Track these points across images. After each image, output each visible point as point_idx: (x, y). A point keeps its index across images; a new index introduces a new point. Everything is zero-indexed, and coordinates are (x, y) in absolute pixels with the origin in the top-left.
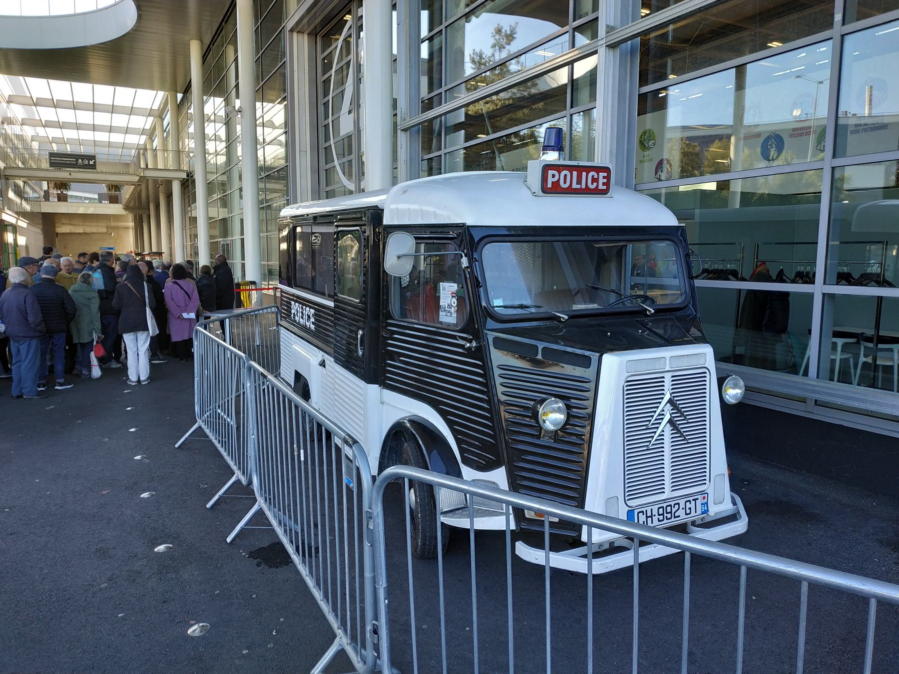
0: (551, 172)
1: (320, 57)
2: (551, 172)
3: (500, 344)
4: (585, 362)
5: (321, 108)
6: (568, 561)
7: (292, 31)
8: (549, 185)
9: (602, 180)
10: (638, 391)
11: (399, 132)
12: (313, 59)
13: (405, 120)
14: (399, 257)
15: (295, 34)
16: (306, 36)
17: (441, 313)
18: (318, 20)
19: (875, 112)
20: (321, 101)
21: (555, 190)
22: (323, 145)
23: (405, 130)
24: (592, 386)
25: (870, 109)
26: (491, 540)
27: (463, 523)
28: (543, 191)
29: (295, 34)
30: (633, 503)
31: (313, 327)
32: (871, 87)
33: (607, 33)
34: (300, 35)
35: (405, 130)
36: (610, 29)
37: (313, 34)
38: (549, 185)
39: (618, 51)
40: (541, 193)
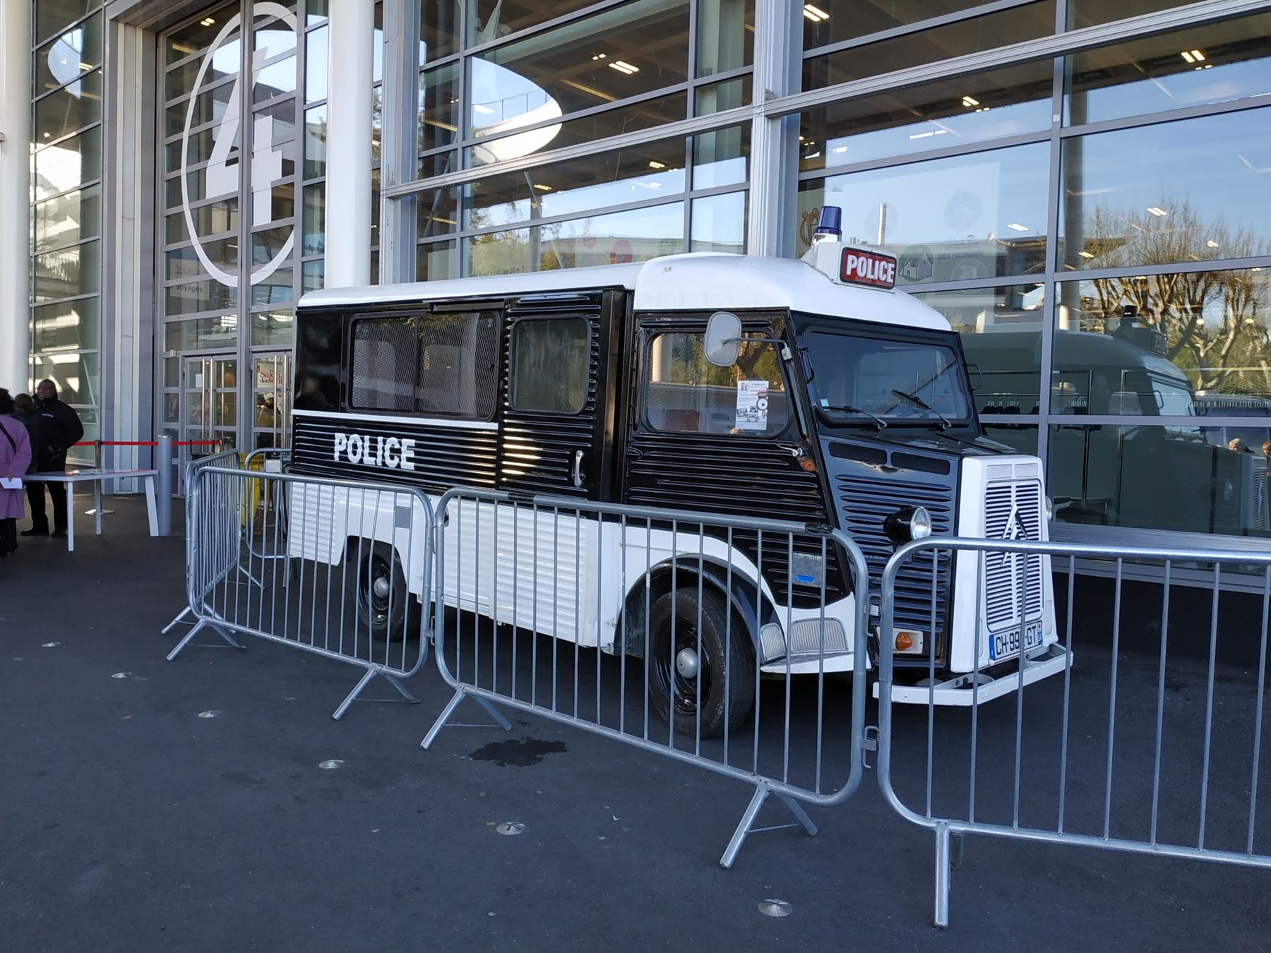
0: (851, 257)
1: (164, 69)
2: (851, 257)
3: (837, 450)
4: (943, 468)
5: (163, 153)
6: (947, 696)
7: (115, 20)
8: (849, 273)
9: (890, 273)
10: (996, 497)
11: (383, 201)
12: (151, 72)
13: (393, 183)
14: (725, 343)
15: (121, 27)
16: (140, 34)
17: (737, 419)
18: (162, 16)
19: (888, 241)
20: (163, 140)
21: (849, 278)
22: (164, 211)
23: (393, 198)
24: (952, 494)
25: (883, 237)
26: (839, 683)
27: (811, 668)
28: (842, 279)
29: (121, 27)
30: (993, 627)
31: (410, 466)
32: (885, 207)
33: (767, 99)
34: (130, 30)
35: (393, 198)
36: (769, 96)
37: (154, 32)
38: (849, 273)
39: (778, 123)
40: (839, 281)
